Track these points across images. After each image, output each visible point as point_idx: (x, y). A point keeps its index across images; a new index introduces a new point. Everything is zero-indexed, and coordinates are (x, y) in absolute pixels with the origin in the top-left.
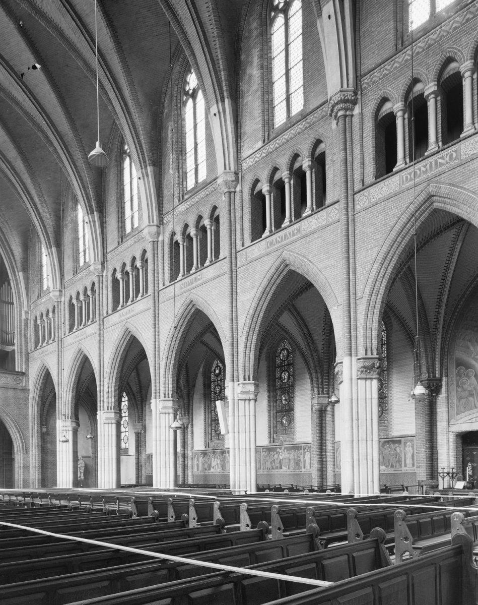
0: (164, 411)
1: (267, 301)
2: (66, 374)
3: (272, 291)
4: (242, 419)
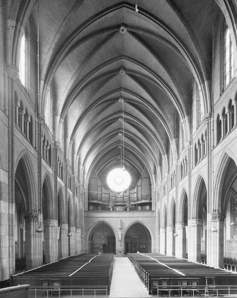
0: (169, 230)
1: (198, 189)
2: (214, 175)
3: (199, 186)
4: (192, 233)
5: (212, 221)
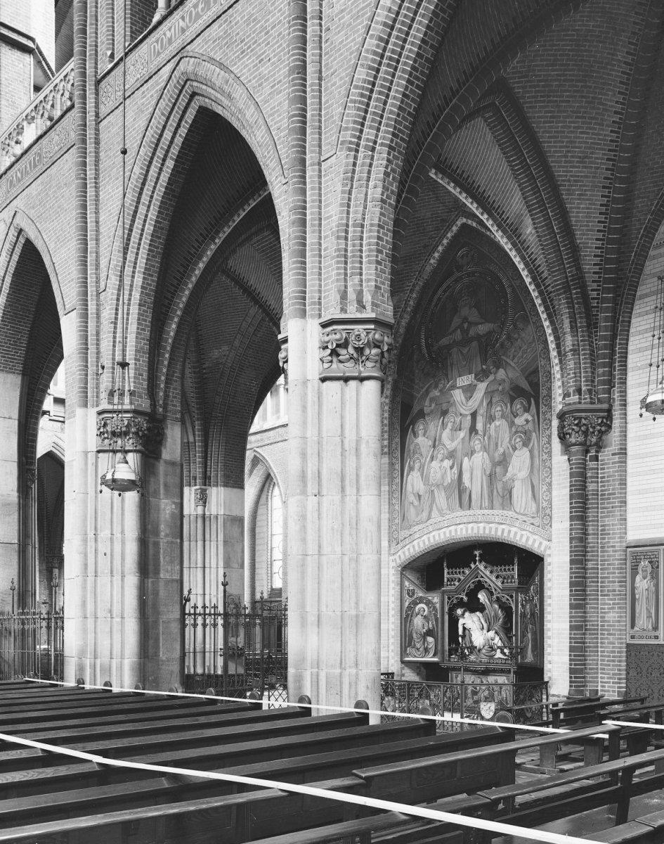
5: (337, 369)
